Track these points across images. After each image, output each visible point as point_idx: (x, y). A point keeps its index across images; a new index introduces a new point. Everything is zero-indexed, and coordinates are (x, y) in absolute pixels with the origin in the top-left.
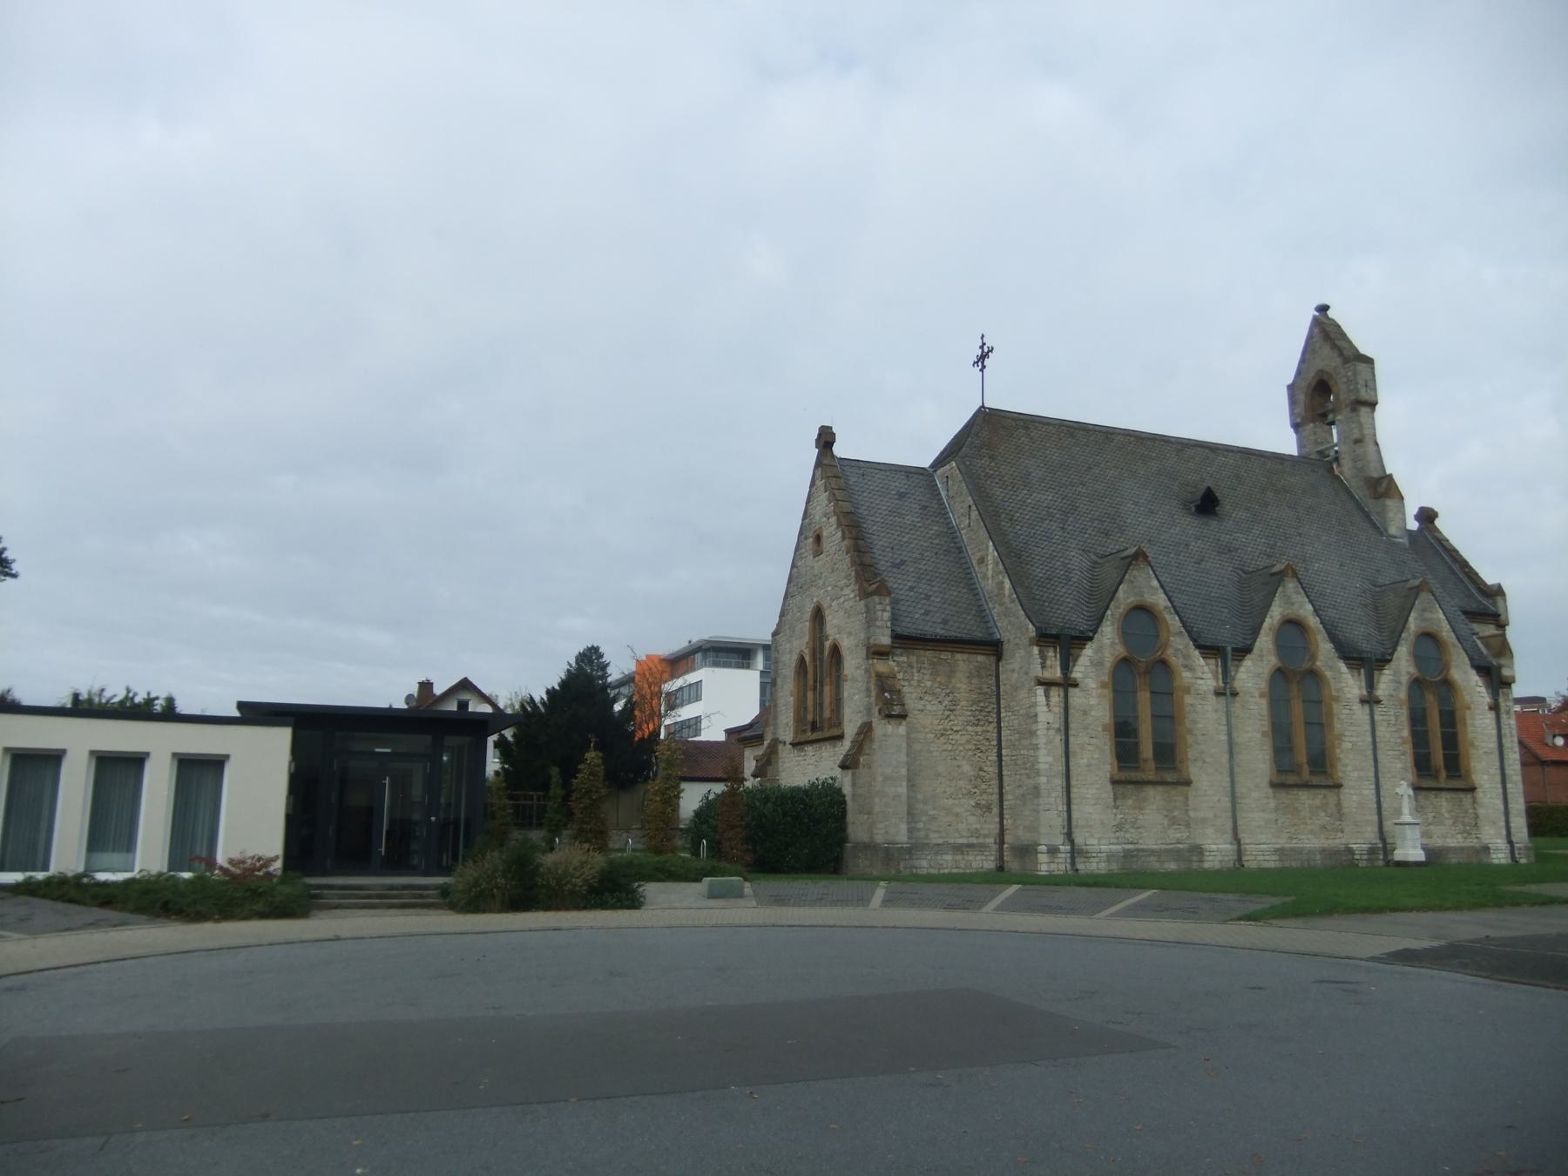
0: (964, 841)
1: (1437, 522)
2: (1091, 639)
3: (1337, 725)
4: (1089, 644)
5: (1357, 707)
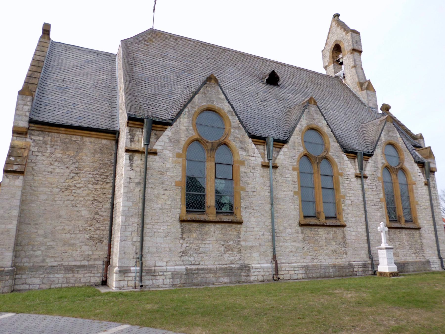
0: (78, 263)
1: (390, 111)
3: (342, 190)
4: (169, 128)
5: (354, 180)
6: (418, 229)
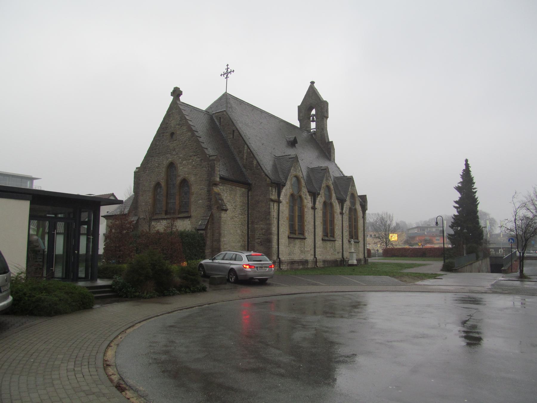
5: (339, 215)
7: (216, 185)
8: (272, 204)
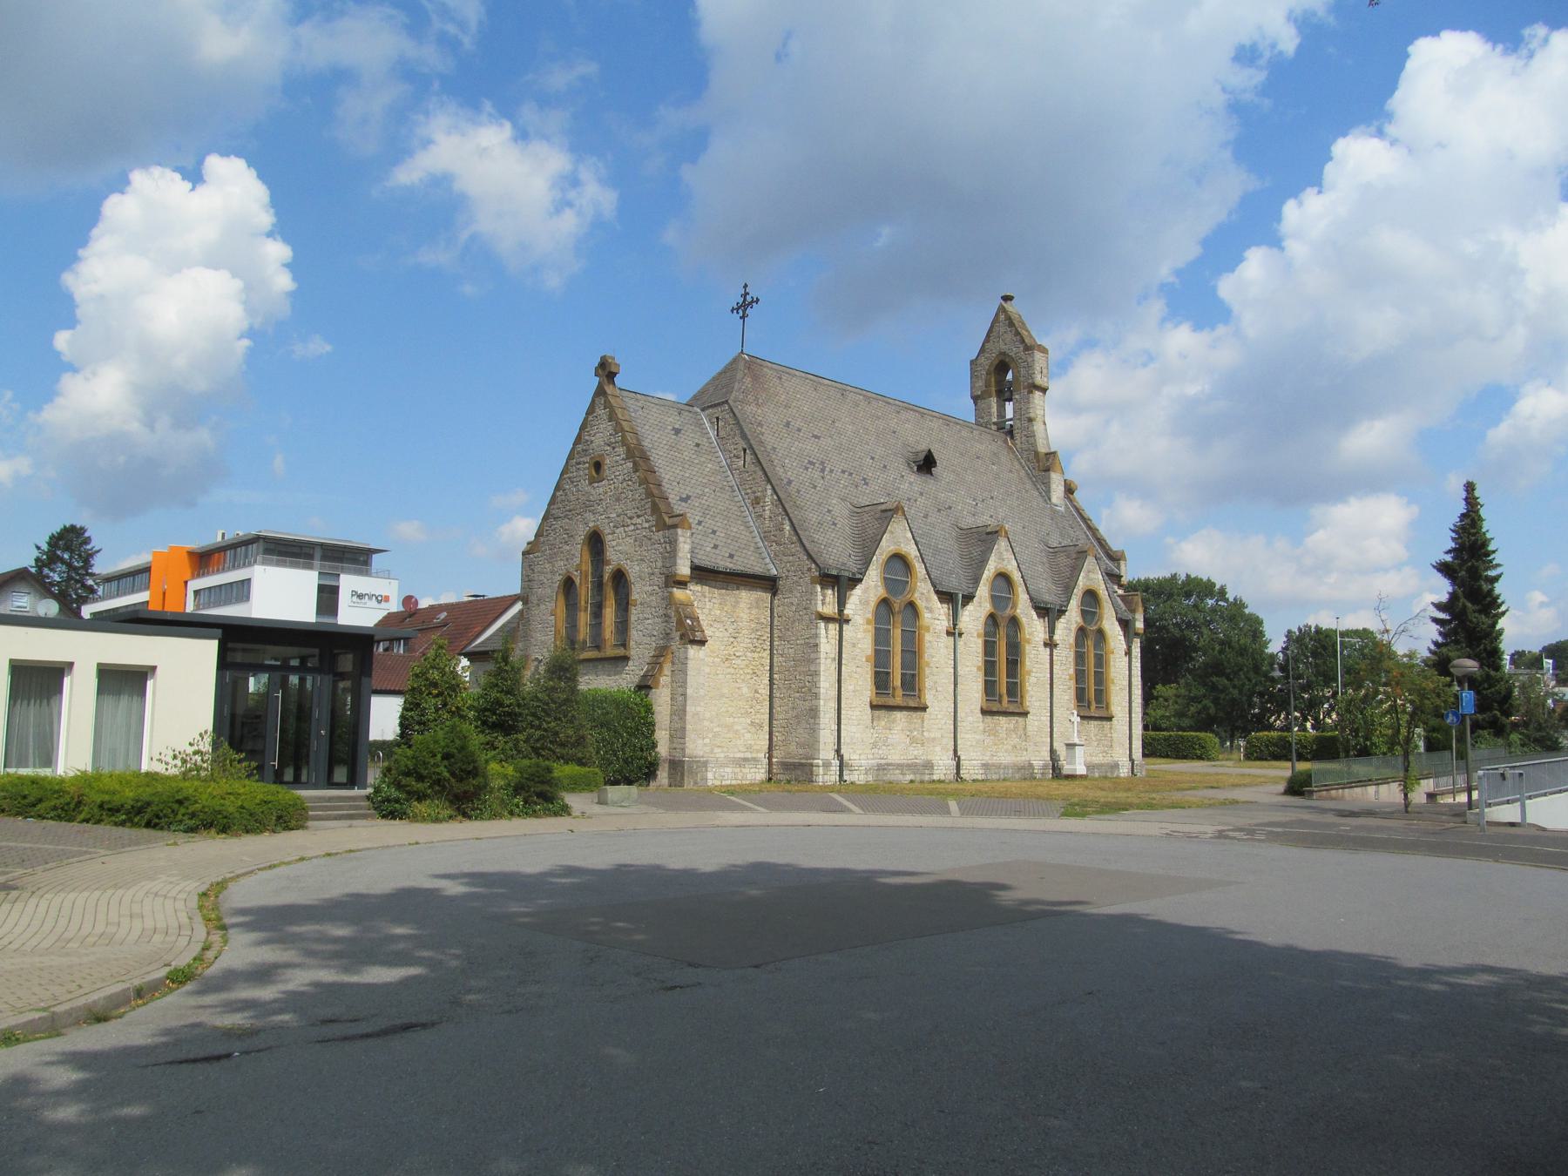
2: (860, 580)
5: (1042, 648)
6: (1025, 714)
7: (682, 584)
8: (822, 625)
